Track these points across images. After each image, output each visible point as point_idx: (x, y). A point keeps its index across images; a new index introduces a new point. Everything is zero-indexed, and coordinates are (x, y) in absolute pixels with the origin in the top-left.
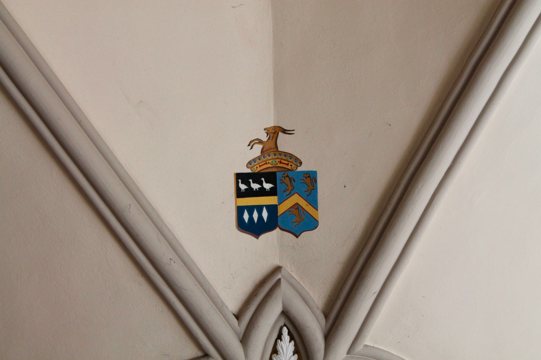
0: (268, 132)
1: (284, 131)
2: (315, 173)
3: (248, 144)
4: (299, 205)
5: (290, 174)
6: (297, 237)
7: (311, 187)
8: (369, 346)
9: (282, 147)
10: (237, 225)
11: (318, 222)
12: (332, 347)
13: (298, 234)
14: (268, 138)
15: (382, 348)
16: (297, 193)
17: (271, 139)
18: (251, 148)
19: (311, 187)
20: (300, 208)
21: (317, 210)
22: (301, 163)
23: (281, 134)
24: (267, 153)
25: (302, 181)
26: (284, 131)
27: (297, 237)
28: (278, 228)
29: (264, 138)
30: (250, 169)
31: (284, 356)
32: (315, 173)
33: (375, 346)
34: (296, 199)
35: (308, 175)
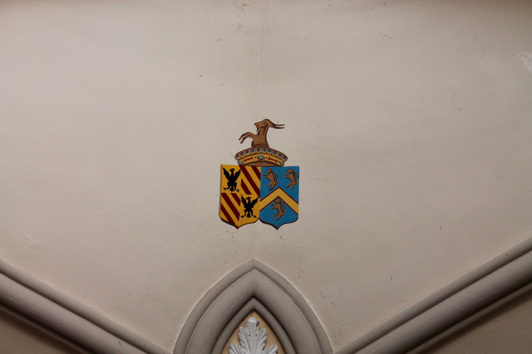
0: (258, 127)
1: (274, 126)
2: (298, 168)
3: (239, 138)
4: (281, 199)
5: (274, 169)
6: (277, 228)
7: (294, 183)
8: (175, 348)
9: (272, 145)
10: (220, 208)
11: (298, 214)
12: (217, 290)
13: (278, 227)
14: (258, 132)
15: (178, 335)
16: (270, 126)
17: (262, 133)
18: (241, 143)
19: (294, 183)
20: (282, 202)
21: (298, 203)
22: (286, 158)
23: (270, 129)
24: (258, 147)
25: (286, 176)
26: (274, 126)
27: (277, 228)
28: (251, 147)
29: (254, 131)
30: (285, 162)
31: (242, 334)
32: (298, 168)
33: (175, 342)
34: (279, 193)
35: (291, 171)
